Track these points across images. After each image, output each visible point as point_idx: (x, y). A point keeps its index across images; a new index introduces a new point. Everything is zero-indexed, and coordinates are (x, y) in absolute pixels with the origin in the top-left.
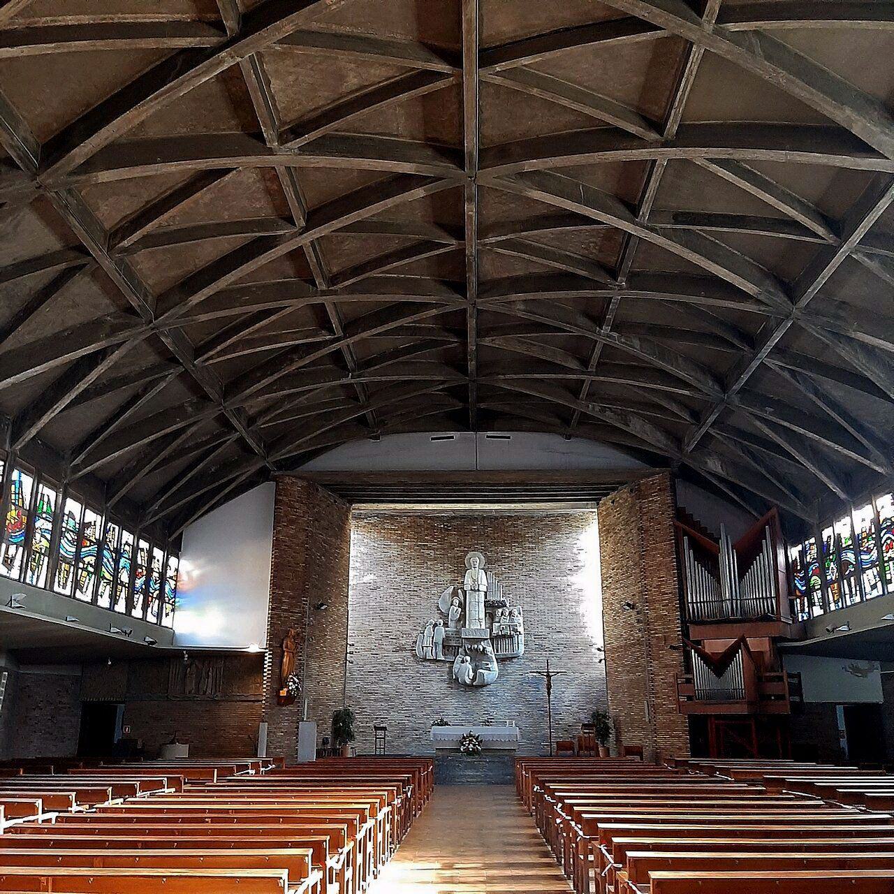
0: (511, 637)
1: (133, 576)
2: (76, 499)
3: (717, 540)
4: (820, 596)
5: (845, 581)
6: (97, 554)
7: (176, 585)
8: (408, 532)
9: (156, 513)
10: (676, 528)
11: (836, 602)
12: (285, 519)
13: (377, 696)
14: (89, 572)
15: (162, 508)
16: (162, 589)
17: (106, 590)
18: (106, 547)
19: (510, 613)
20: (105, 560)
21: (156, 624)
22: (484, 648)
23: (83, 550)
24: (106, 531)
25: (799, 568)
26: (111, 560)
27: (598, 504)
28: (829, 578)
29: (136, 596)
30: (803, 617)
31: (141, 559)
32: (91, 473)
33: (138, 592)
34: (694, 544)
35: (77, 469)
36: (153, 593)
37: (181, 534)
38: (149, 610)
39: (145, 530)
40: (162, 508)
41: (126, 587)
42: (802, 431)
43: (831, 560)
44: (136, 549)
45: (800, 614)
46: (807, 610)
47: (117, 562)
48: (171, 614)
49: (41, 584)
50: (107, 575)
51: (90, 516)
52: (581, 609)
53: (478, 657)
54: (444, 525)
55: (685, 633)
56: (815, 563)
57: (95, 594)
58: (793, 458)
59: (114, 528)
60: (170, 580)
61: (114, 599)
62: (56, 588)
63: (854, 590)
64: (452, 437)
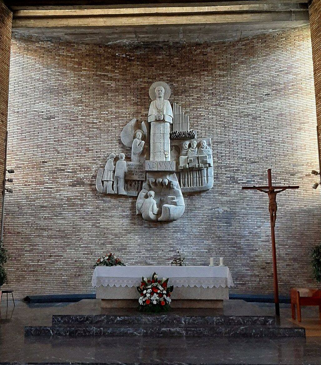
0: (200, 170)
19: (199, 145)
54: (126, 55)
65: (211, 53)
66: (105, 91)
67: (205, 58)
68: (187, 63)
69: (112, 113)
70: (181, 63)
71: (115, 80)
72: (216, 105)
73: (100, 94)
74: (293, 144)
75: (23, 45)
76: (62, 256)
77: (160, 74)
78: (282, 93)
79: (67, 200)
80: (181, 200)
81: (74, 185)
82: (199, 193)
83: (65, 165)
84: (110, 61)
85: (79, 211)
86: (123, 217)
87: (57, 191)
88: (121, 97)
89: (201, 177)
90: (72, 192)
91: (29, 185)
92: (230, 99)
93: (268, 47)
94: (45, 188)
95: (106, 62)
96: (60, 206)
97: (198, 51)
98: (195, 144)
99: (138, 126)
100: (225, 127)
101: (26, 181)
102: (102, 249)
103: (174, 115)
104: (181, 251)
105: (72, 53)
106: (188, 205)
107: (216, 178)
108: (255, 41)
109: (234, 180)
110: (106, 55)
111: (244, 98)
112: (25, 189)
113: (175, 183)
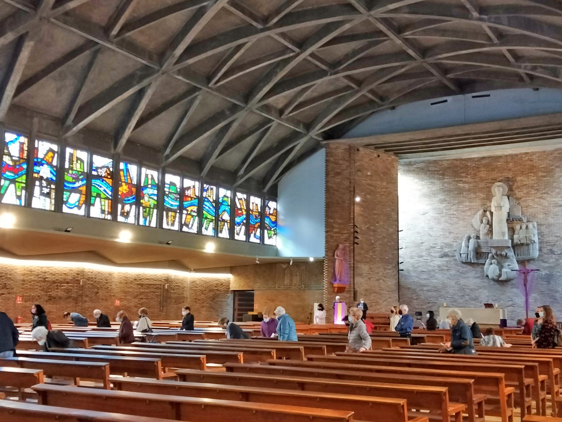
0: (528, 245)
8: (448, 172)
13: (428, 288)
14: (193, 216)
19: (527, 227)
21: (260, 243)
22: (506, 254)
26: (211, 207)
35: (168, 157)
49: (153, 224)
51: (188, 183)
53: (501, 258)
54: (476, 164)
62: (165, 226)
64: (446, 101)
65: (535, 159)
66: (460, 191)
67: (531, 163)
68: (519, 167)
70: (515, 167)
71: (468, 183)
72: (539, 198)
73: (458, 194)
75: (406, 168)
76: (436, 303)
79: (438, 267)
80: (516, 266)
81: (442, 257)
82: (529, 261)
83: (435, 244)
84: (464, 170)
85: (446, 274)
87: (431, 261)
89: (529, 250)
90: (441, 261)
91: (413, 258)
92: (549, 194)
94: (424, 259)
95: (462, 170)
96: (433, 271)
97: (527, 158)
98: (524, 227)
100: (546, 214)
101: (412, 256)
102: (462, 299)
103: (510, 206)
104: (516, 301)
107: (540, 250)
109: (552, 252)
110: (461, 166)
112: (412, 261)
113: (511, 253)
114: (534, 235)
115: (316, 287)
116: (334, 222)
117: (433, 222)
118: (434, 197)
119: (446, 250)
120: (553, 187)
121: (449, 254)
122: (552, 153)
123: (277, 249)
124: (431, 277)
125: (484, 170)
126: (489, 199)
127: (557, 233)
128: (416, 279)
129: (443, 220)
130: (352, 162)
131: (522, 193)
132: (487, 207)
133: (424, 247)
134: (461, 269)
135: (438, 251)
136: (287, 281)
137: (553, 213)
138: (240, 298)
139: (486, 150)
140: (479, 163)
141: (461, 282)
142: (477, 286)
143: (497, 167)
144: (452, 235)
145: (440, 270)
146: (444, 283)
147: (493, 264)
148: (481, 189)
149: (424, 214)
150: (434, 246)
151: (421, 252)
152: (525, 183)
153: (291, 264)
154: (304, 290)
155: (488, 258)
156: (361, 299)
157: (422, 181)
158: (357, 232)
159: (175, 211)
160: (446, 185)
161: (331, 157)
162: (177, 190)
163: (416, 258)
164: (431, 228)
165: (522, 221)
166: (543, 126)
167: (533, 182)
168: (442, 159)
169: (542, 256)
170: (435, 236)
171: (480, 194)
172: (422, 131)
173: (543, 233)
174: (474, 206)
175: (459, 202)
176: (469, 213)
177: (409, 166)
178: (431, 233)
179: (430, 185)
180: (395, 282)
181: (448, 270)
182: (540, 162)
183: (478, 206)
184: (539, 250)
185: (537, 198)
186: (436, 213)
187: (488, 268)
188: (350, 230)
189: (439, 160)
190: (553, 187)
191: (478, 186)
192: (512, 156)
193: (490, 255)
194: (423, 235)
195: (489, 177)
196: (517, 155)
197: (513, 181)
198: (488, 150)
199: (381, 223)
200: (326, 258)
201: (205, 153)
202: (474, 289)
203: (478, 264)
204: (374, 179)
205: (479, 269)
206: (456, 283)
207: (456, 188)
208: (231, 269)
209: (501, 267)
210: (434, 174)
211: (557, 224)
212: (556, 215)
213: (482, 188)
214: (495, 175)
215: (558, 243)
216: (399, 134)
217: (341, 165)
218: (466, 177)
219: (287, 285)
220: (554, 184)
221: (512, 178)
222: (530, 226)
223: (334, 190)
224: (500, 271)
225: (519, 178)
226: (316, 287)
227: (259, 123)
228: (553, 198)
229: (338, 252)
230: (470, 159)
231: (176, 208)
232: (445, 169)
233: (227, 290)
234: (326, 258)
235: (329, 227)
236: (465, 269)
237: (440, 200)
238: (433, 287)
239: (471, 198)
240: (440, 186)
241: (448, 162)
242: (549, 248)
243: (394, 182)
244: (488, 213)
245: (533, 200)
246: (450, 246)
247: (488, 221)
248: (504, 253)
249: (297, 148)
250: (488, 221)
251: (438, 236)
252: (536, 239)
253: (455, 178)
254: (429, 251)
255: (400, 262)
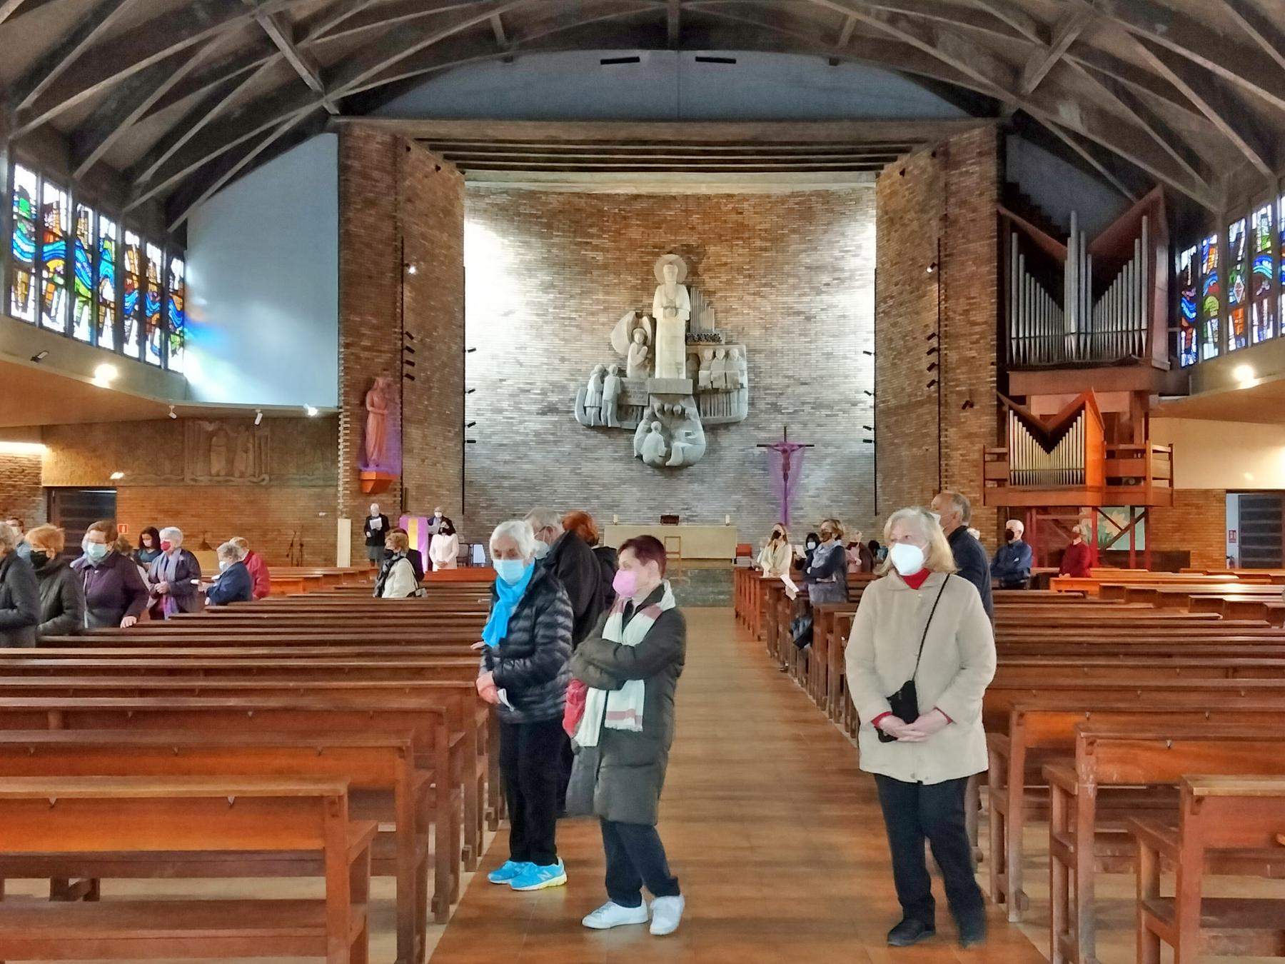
0: (728, 392)
1: (121, 289)
2: (28, 166)
3: (1063, 238)
4: (1215, 326)
5: (1255, 305)
6: (66, 255)
7: (183, 304)
8: (559, 221)
9: (148, 187)
10: (1000, 218)
11: (1237, 337)
12: (358, 199)
13: (513, 482)
14: (57, 286)
15: (160, 176)
16: (163, 311)
17: (84, 314)
18: (77, 244)
19: (727, 355)
20: (78, 265)
21: (160, 367)
22: (683, 410)
23: (46, 249)
24: (76, 217)
25: (1189, 283)
26: (85, 265)
27: (878, 176)
28: (1231, 300)
29: (127, 323)
30: (1187, 360)
31: (131, 263)
32: (48, 124)
33: (130, 316)
34: (1027, 245)
35: (26, 116)
36: (151, 317)
37: (185, 223)
38: (148, 344)
39: (135, 214)
40: (160, 176)
41: (111, 308)
42: (1209, 65)
43: (1238, 272)
44: (123, 248)
45: (1184, 356)
46: (1194, 348)
47: (95, 267)
48: (180, 351)
50: (83, 290)
51: (52, 194)
52: (839, 347)
53: (671, 418)
54: (620, 210)
55: (1002, 384)
56: (1214, 275)
57: (71, 322)
58: (1193, 108)
59: (86, 213)
60: (175, 298)
61: (97, 328)
62: (15, 312)
63: (1265, 319)
64: (636, 60)
66: (586, 268)
68: (713, 224)
69: (598, 302)
70: (704, 224)
71: (602, 250)
72: (754, 294)
73: (579, 273)
74: (856, 360)
77: (672, 241)
78: (846, 284)
79: (535, 436)
80: (700, 435)
81: (544, 413)
82: (727, 426)
84: (594, 220)
85: (551, 451)
86: (615, 459)
87: (521, 422)
88: (612, 277)
90: (542, 422)
91: (482, 415)
92: (774, 286)
93: (832, 211)
94: (504, 418)
96: (525, 443)
97: (730, 206)
98: (720, 354)
99: (636, 323)
100: (766, 329)
101: (479, 409)
103: (692, 307)
104: (698, 509)
105: (538, 210)
106: (710, 444)
107: (752, 404)
108: (813, 198)
109: (776, 408)
110: (589, 209)
111: (794, 287)
113: (692, 410)
114: (742, 371)
115: (300, 480)
116: (362, 324)
117: (527, 334)
118: (530, 277)
119: (554, 398)
120: (783, 274)
121: (560, 406)
122: (783, 200)
123: (187, 383)
124: (520, 458)
125: (637, 225)
126: (648, 289)
127: (788, 369)
128: (487, 463)
129: (547, 329)
130: (399, 176)
131: (717, 282)
132: (644, 306)
133: (505, 390)
134: (585, 442)
135: (536, 399)
136: (217, 465)
137: (782, 328)
138: (68, 506)
139: (657, 181)
140: (628, 208)
141: (583, 470)
142: (618, 479)
143: (665, 221)
144: (566, 366)
145: (538, 443)
146: (548, 471)
147: (654, 431)
148: (630, 268)
149: (506, 314)
150: (528, 387)
151: (499, 401)
152: (724, 260)
153: (257, 422)
154: (266, 488)
155: (642, 419)
156: (437, 509)
157: (503, 237)
158: (411, 351)
159: (28, 271)
160: (554, 251)
161: (355, 158)
162: (30, 211)
163: (489, 415)
164: (522, 348)
165: (719, 340)
166: (848, 143)
167: (741, 259)
168: (549, 190)
169: (756, 415)
170: (531, 366)
171: (629, 278)
172: (601, 123)
173: (760, 368)
174: (614, 302)
175: (582, 292)
176: (603, 319)
177: (475, 200)
178: (522, 358)
179: (519, 247)
180: (454, 470)
181: (556, 442)
182: (758, 218)
183: (624, 303)
184: (749, 404)
185: (749, 294)
186: (532, 314)
187: (642, 440)
188: (395, 344)
189: (541, 192)
190: (783, 274)
191: (625, 259)
192: (697, 198)
193: (647, 412)
194: (504, 363)
195: (647, 240)
196: (708, 197)
197: (698, 254)
198: (663, 181)
199: (440, 330)
200: (346, 410)
201: (91, 115)
202: (611, 484)
203: (620, 430)
204: (431, 223)
205: (621, 441)
206: (573, 471)
207: (576, 260)
208: (45, 434)
209: (669, 437)
210: (530, 222)
211: (788, 350)
212: (789, 333)
213: (631, 264)
214: (661, 236)
215: (790, 390)
216: (536, 123)
217: (377, 181)
218: (599, 237)
219: (218, 475)
220: (787, 268)
221: (697, 247)
222: (735, 352)
223: (362, 243)
224: (668, 445)
225: (712, 249)
226: (300, 480)
227: (235, 53)
228: (782, 295)
229: (373, 397)
230: (608, 195)
231: (30, 261)
232: (554, 214)
233: (35, 487)
234: (346, 410)
235: (349, 333)
236: (592, 442)
237: (542, 283)
238: (525, 480)
239: (608, 285)
240: (542, 253)
241: (561, 198)
242: (770, 399)
243: (458, 234)
244: (645, 320)
245: (741, 298)
246: (563, 388)
247: (646, 337)
248: (678, 408)
249: (286, 128)
250: (646, 337)
251: (536, 367)
252: (744, 380)
253: (575, 237)
254: (517, 399)
255: (467, 422)
